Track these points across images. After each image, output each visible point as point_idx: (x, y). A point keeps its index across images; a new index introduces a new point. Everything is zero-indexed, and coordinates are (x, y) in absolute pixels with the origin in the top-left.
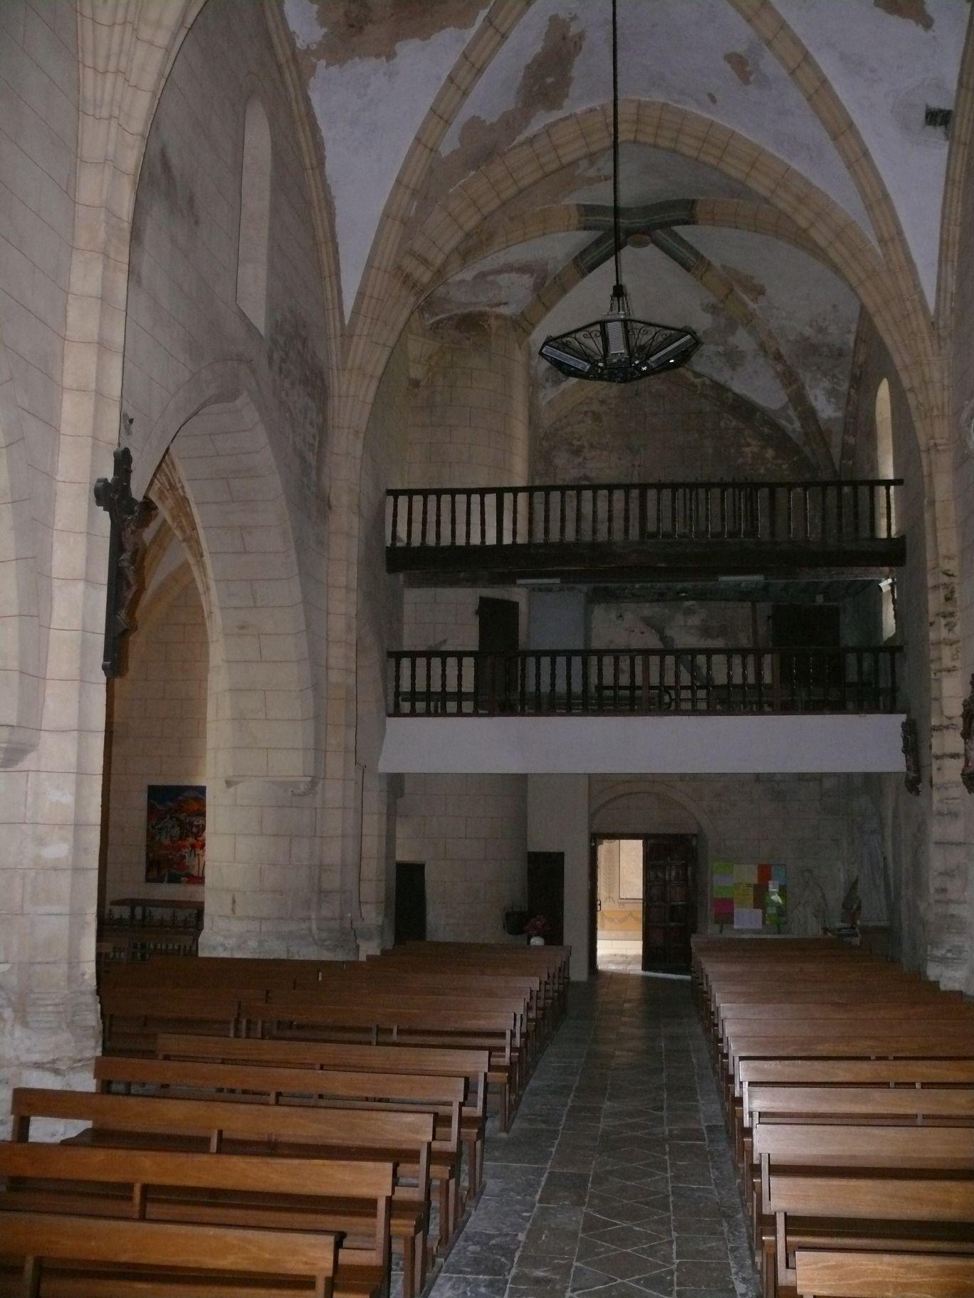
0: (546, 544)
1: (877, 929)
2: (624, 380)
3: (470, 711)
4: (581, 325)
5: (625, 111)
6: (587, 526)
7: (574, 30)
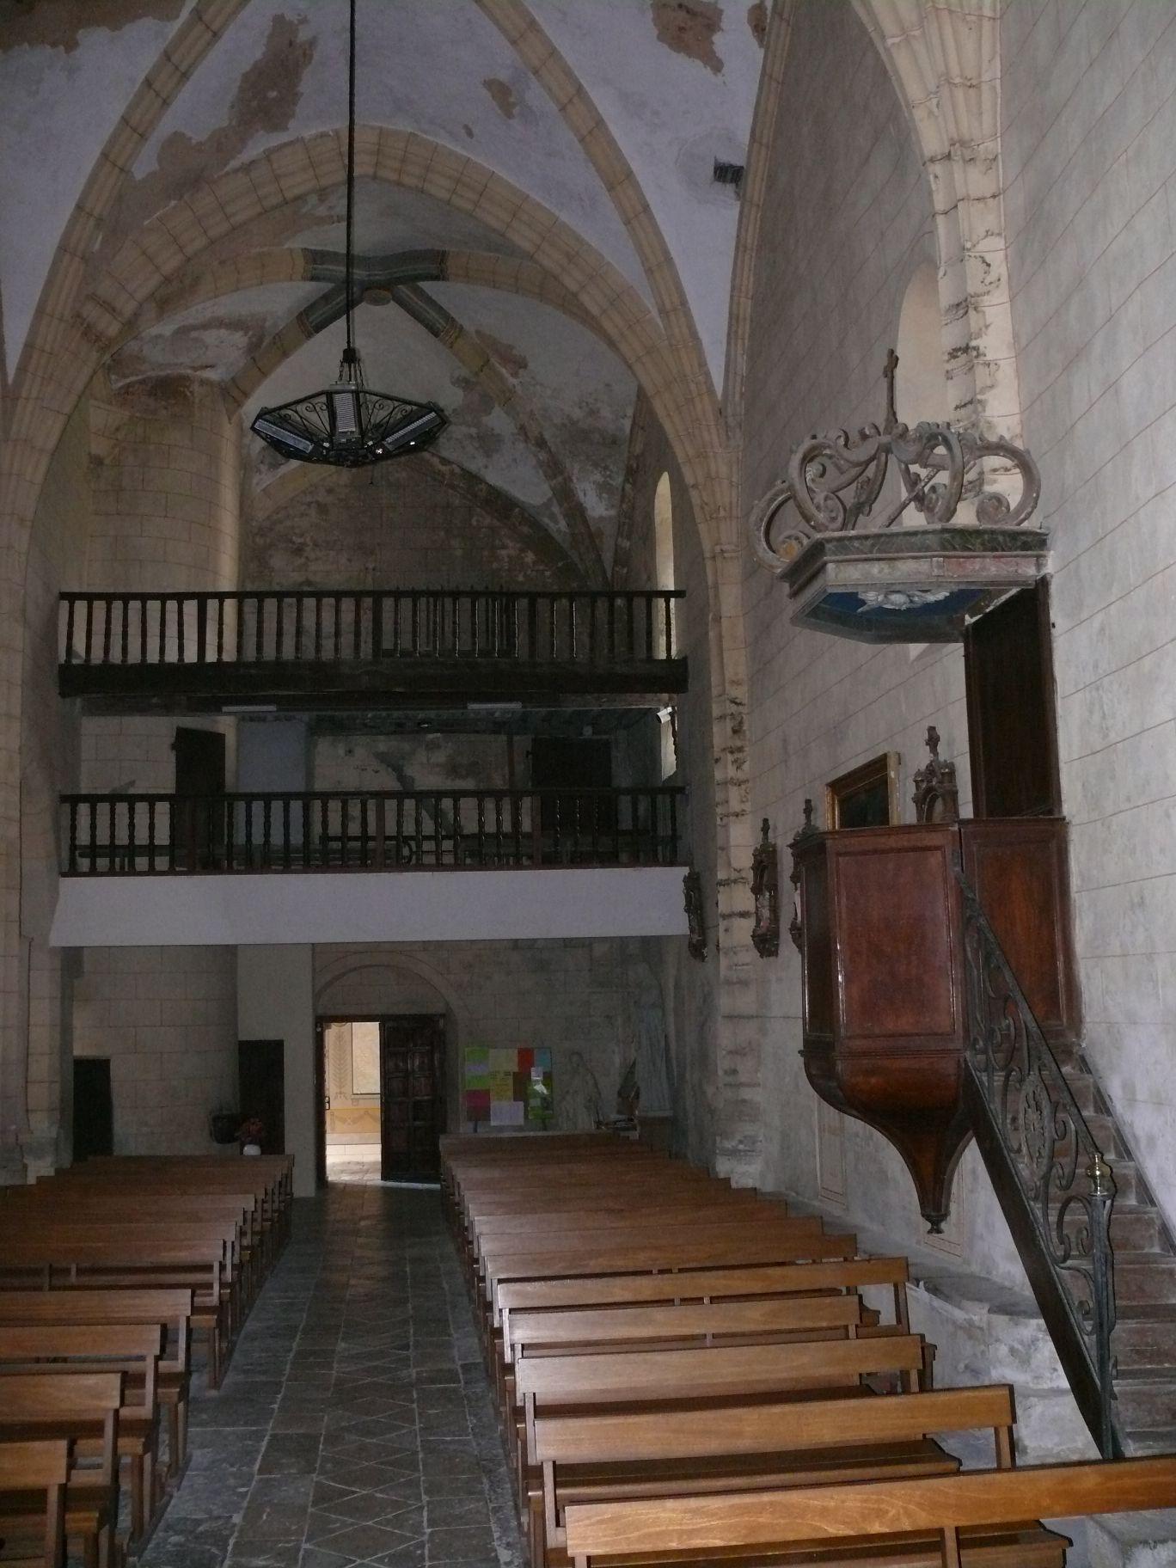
0: (259, 663)
1: (663, 1120)
2: (355, 464)
3: (165, 868)
4: (302, 396)
5: (363, 139)
6: (308, 642)
7: (303, 35)
